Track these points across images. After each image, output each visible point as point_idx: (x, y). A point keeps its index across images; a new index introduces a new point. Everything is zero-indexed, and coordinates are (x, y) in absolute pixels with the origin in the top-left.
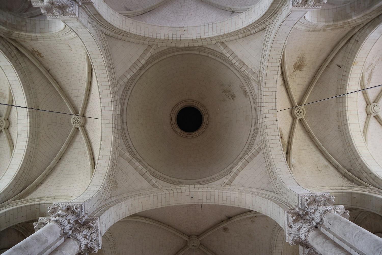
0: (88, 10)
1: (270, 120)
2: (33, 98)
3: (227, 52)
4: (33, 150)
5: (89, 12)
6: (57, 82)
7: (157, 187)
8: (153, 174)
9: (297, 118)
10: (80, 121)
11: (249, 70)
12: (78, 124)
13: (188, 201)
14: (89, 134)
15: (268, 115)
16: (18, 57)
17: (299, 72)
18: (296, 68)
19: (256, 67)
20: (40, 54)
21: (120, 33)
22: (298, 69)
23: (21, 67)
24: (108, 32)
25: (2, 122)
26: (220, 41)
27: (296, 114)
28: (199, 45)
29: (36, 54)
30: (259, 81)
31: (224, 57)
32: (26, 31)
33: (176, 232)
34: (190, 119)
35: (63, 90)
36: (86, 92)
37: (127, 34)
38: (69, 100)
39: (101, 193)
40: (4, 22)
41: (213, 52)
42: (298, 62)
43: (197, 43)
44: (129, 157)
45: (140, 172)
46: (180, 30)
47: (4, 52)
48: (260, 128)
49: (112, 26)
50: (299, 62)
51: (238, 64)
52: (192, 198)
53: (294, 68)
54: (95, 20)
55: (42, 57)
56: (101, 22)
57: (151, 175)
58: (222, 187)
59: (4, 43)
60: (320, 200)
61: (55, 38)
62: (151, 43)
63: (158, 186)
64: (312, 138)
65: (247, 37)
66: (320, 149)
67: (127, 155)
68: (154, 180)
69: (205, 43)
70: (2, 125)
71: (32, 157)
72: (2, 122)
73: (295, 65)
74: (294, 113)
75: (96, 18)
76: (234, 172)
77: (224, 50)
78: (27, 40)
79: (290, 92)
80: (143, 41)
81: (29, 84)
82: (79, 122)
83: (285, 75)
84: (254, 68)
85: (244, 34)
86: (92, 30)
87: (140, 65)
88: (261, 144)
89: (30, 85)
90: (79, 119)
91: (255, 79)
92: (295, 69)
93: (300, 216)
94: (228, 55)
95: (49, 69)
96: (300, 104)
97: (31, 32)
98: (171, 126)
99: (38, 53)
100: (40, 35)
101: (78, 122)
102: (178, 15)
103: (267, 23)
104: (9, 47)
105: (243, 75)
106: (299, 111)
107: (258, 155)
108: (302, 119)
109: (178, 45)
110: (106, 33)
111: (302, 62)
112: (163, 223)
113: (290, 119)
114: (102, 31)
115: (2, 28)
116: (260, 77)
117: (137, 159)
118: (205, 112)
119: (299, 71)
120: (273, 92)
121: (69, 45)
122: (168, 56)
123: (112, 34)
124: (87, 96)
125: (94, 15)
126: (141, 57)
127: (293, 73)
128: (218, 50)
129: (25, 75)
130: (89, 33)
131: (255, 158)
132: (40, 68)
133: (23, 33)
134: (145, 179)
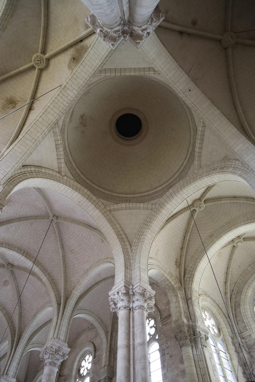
0: (129, 280)
1: (73, 89)
2: (207, 244)
3: (62, 163)
4: (241, 219)
5: (129, 273)
6: (185, 237)
7: (203, 123)
8: (196, 130)
9: (45, 58)
10: (198, 205)
11: (56, 137)
12: (201, 205)
13: (196, 91)
14: (203, 192)
15: (71, 94)
16: (188, 272)
17: (14, 97)
18: (15, 103)
19: (49, 137)
20: (176, 262)
21: (121, 239)
22: (14, 100)
23: (193, 265)
24: (128, 247)
25: (237, 243)
26: (61, 176)
27: (43, 63)
28: (77, 183)
29: (178, 264)
30: (55, 124)
31: (66, 159)
32: (170, 282)
33: (230, 66)
34: (128, 126)
35: (187, 230)
36: (176, 217)
37: (119, 235)
38: (190, 221)
39: (239, 172)
40: (175, 297)
41: (71, 169)
42: (10, 108)
43: (77, 186)
44: (197, 160)
45: (201, 143)
46: (82, 205)
47: (192, 282)
48: (86, 87)
49: (124, 252)
50: (9, 107)
51: (61, 149)
52: (190, 90)
53: (16, 105)
54: (130, 263)
55: (177, 259)
56: (127, 259)
57: (198, 133)
58: (160, 73)
59: (187, 285)
60: (101, 33)
61: (160, 265)
62: (108, 213)
63: (202, 123)
64: (46, 28)
65: (39, 165)
66: (46, 10)
67: (196, 163)
68: (200, 128)
69: (72, 182)
70: (239, 242)
71: (247, 217)
72: (237, 243)
73: (14, 107)
74: (45, 65)
75: (129, 265)
76: (139, 73)
77: (62, 166)
78: (174, 277)
79: (35, 86)
80: (112, 219)
81: (200, 252)
82: (200, 205)
83: (28, 107)
84: (51, 136)
85: (40, 170)
86: (137, 260)
87: (127, 205)
88: (96, 75)
89: (200, 251)
90: (197, 207)
91: (57, 128)
92: (16, 103)
93: (132, 34)
94: (63, 161)
95: (181, 249)
96: (33, 68)
97: (168, 280)
98: (146, 135)
99: (176, 263)
100: (165, 274)
101: (200, 205)
102: (73, 208)
103: (19, 171)
104: (187, 281)
105: (63, 135)
106: (39, 63)
107: (108, 67)
108: (42, 52)
109: (92, 195)
110: (131, 247)
111: (6, 105)
112: (230, 85)
113: (52, 62)
114: (132, 252)
115: (180, 295)
116: (52, 127)
117: (193, 150)
118: (113, 122)
119: (14, 98)
120: (52, 109)
121: (156, 254)
122: (103, 191)
123: (127, 243)
124: (177, 214)
125: (128, 268)
126: (122, 209)
127: (20, 101)
128: (67, 170)
129: (196, 259)
130: (140, 261)
131: (111, 68)
132: (185, 255)
133: (173, 283)
134: (204, 135)
